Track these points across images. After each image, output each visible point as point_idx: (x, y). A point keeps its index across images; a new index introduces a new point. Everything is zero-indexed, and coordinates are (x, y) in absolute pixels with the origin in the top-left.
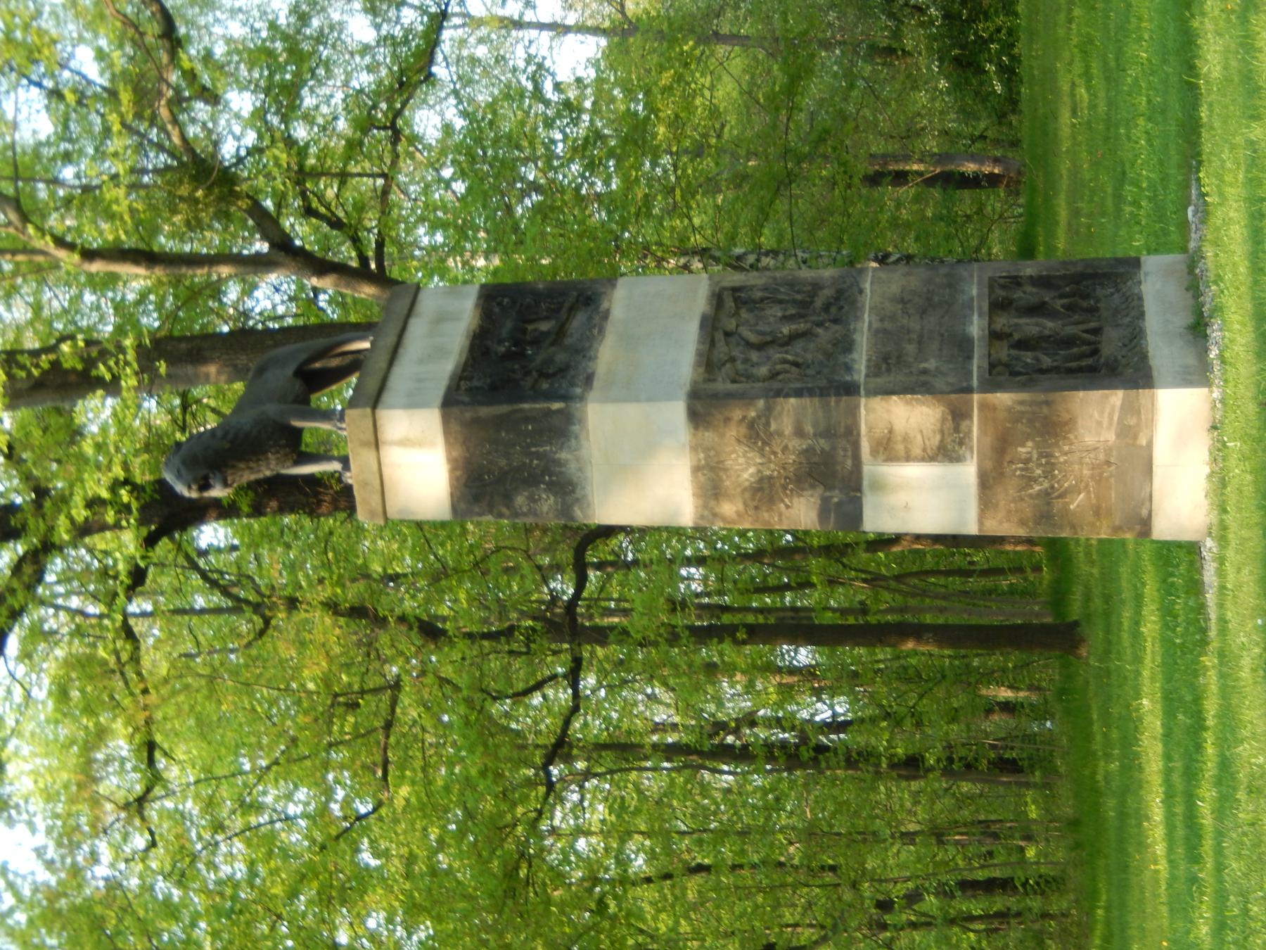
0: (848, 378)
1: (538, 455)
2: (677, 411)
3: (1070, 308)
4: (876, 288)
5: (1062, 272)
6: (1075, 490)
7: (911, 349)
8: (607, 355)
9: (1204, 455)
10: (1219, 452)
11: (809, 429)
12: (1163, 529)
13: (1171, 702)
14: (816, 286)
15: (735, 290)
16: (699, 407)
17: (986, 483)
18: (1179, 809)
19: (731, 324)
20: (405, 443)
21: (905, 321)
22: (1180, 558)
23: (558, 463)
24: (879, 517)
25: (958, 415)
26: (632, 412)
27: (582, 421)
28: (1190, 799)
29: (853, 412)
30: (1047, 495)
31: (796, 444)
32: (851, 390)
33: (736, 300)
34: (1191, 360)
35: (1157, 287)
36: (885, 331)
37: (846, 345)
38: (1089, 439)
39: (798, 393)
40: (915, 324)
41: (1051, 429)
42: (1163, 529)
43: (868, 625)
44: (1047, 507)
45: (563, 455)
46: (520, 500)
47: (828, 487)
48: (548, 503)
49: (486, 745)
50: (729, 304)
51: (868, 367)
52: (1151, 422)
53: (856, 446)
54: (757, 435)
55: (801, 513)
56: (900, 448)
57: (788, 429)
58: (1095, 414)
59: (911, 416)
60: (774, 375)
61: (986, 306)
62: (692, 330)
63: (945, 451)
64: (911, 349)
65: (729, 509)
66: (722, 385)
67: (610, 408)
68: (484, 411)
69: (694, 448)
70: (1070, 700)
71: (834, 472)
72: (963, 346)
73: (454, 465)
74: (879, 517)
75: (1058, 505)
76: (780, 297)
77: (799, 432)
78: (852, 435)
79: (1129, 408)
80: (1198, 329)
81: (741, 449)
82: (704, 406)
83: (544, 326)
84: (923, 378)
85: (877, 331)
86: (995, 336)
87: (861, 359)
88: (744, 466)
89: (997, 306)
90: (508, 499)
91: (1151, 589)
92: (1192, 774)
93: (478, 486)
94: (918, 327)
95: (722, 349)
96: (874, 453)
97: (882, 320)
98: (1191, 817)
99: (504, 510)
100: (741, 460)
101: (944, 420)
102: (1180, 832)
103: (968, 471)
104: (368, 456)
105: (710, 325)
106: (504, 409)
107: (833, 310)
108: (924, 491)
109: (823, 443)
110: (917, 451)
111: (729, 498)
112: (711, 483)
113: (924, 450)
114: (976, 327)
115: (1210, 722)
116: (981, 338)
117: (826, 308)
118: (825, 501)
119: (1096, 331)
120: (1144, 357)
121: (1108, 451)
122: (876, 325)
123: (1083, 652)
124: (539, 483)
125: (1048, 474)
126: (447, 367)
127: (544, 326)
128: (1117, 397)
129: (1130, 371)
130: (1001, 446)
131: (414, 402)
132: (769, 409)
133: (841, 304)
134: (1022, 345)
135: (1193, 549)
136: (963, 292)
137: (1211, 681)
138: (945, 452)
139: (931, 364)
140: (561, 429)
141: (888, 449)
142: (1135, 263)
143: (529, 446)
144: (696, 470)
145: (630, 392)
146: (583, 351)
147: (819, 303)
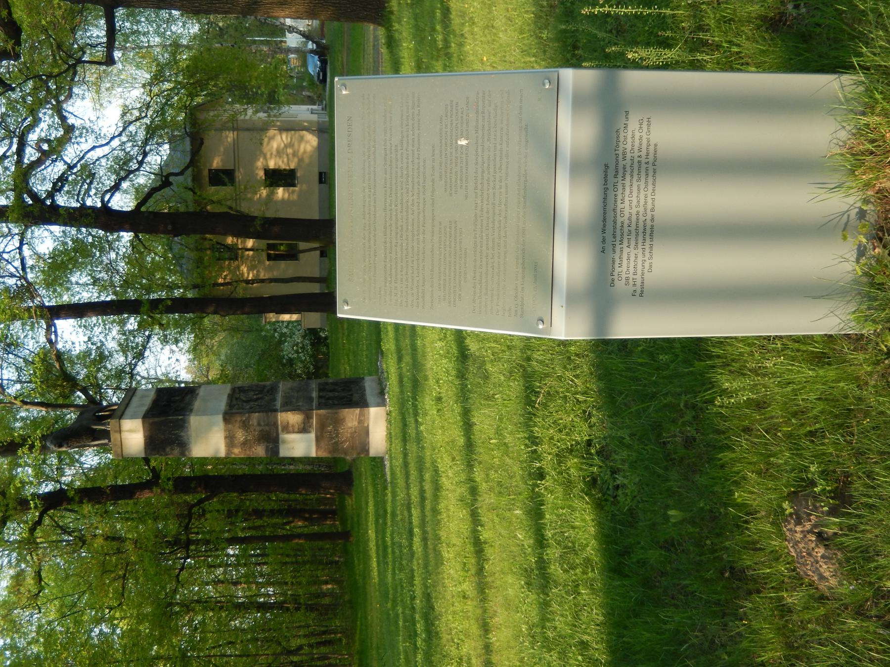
1: (174, 434)
2: (220, 418)
3: (343, 390)
4: (283, 387)
6: (345, 441)
7: (294, 400)
8: (197, 404)
9: (385, 428)
10: (389, 422)
11: (262, 424)
12: (372, 453)
13: (376, 505)
14: (265, 386)
16: (227, 417)
17: (318, 439)
18: (380, 537)
19: (238, 396)
20: (131, 431)
22: (378, 462)
23: (181, 437)
24: (284, 452)
25: (308, 417)
26: (205, 418)
27: (189, 422)
28: (384, 537)
29: (276, 417)
30: (336, 443)
31: (258, 428)
32: (276, 411)
34: (380, 401)
35: (369, 384)
37: (274, 400)
38: (350, 425)
39: (259, 412)
41: (338, 422)
42: (372, 453)
44: (335, 447)
45: (182, 434)
47: (268, 442)
50: (237, 391)
52: (368, 418)
53: (277, 428)
54: (245, 426)
55: (260, 451)
56: (291, 429)
57: (255, 424)
58: (350, 417)
59: (293, 418)
60: (251, 408)
62: (225, 398)
63: (304, 429)
64: (294, 400)
65: (236, 451)
66: (234, 411)
67: (198, 418)
68: (156, 420)
69: (225, 431)
70: (346, 552)
71: (271, 438)
72: (311, 399)
73: (145, 436)
74: (284, 452)
75: (340, 446)
77: (259, 424)
78: (275, 424)
79: (361, 414)
80: (382, 393)
81: (240, 431)
82: (228, 417)
83: (177, 398)
86: (320, 397)
87: (278, 404)
88: (240, 435)
89: (320, 390)
90: (164, 450)
91: (370, 488)
92: (385, 556)
93: (153, 443)
95: (235, 402)
96: (283, 431)
98: (384, 542)
102: (381, 553)
103: (312, 436)
104: (117, 435)
105: (231, 397)
106: (163, 419)
108: (299, 445)
109: (267, 428)
110: (296, 430)
111: (236, 447)
112: (230, 440)
114: (314, 395)
115: (389, 511)
118: (267, 447)
119: (351, 395)
120: (366, 400)
121: (355, 428)
123: (351, 539)
125: (337, 436)
126: (145, 409)
127: (177, 398)
128: (358, 411)
129: (362, 403)
130: (322, 427)
131: (133, 417)
132: (249, 417)
133: (273, 390)
134: (329, 399)
135: (382, 459)
137: (389, 497)
138: (304, 430)
139: (300, 404)
140: (182, 425)
141: (287, 429)
142: (363, 378)
144: (226, 438)
145: (204, 413)
146: (190, 403)
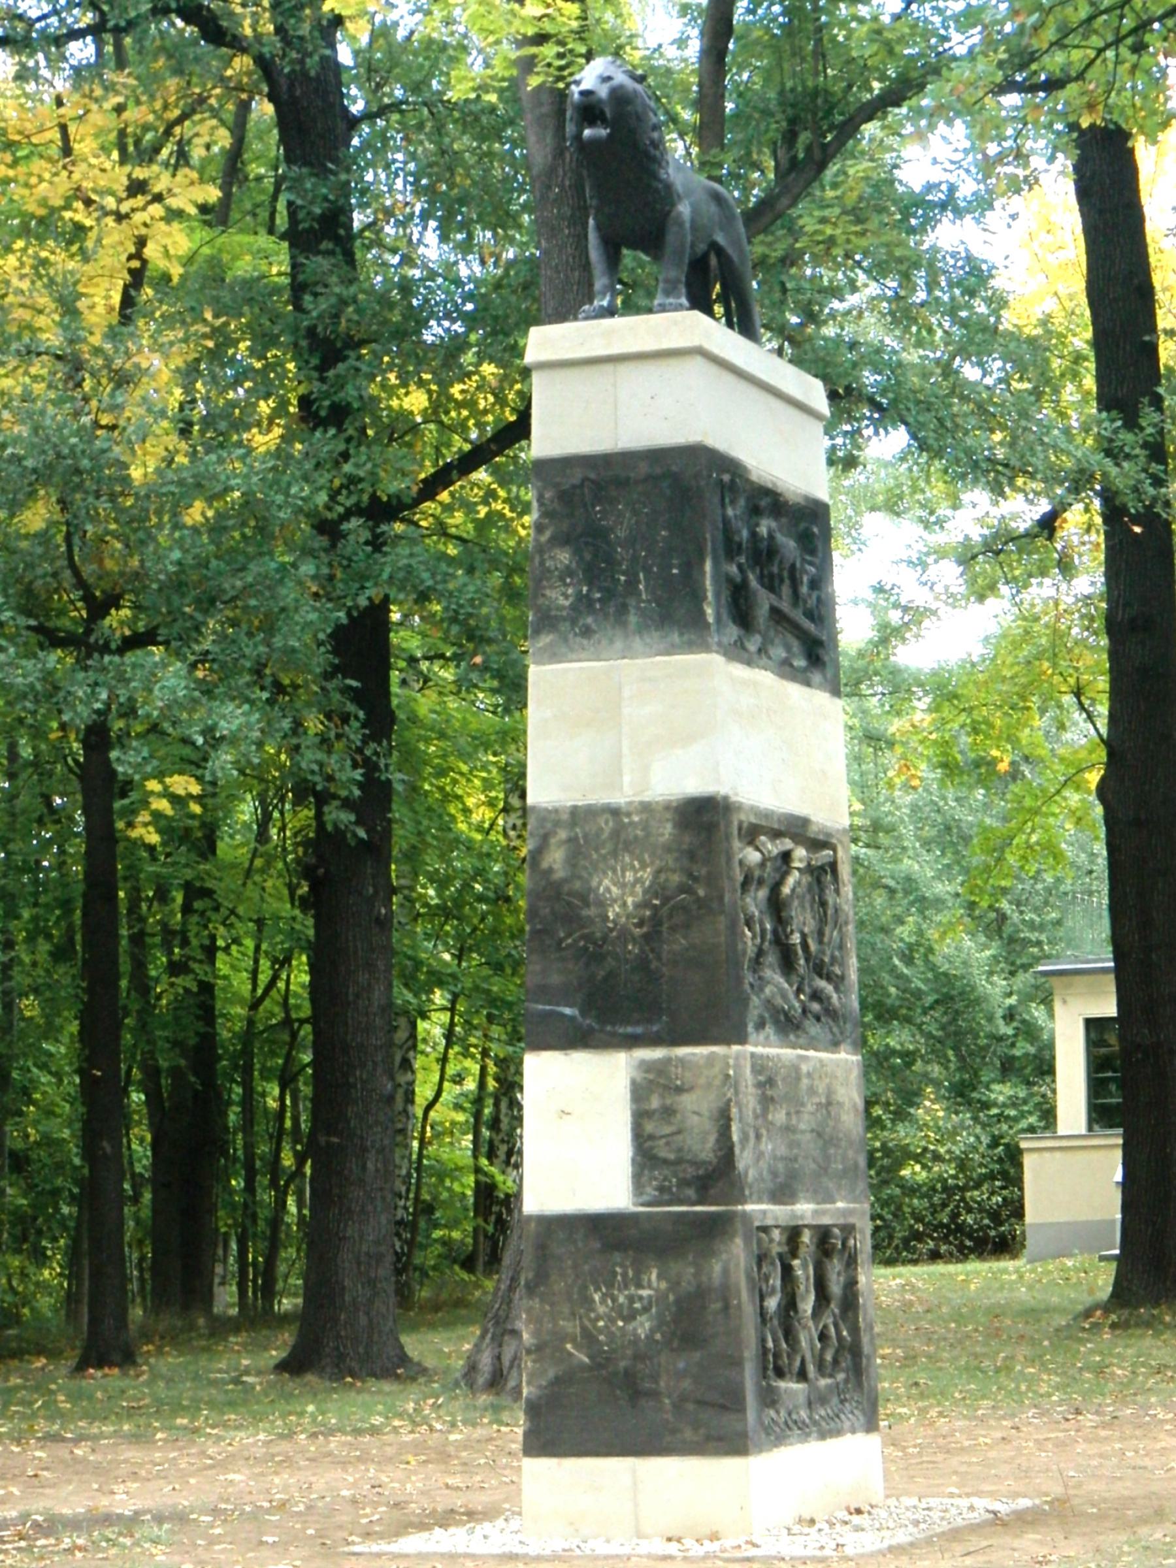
0: (750, 1028)
1: (632, 583)
5: (862, 1325)
15: (833, 866)
21: (810, 1108)
33: (822, 868)
36: (798, 1079)
40: (805, 1123)
43: (314, 1020)
46: (564, 557)
48: (560, 597)
49: (928, 554)
51: (761, 1056)
61: (826, 1221)
76: (827, 930)
84: (752, 1135)
85: (797, 1069)
89: (823, 1235)
94: (802, 1126)
97: (809, 1075)
99: (548, 534)
100: (629, 876)
101: (696, 1164)
107: (816, 1007)
110: (649, 1127)
113: (651, 1137)
114: (805, 1209)
116: (794, 1215)
117: (816, 996)
122: (804, 1068)
124: (590, 584)
136: (839, 1187)
143: (647, 570)
147: (822, 984)
